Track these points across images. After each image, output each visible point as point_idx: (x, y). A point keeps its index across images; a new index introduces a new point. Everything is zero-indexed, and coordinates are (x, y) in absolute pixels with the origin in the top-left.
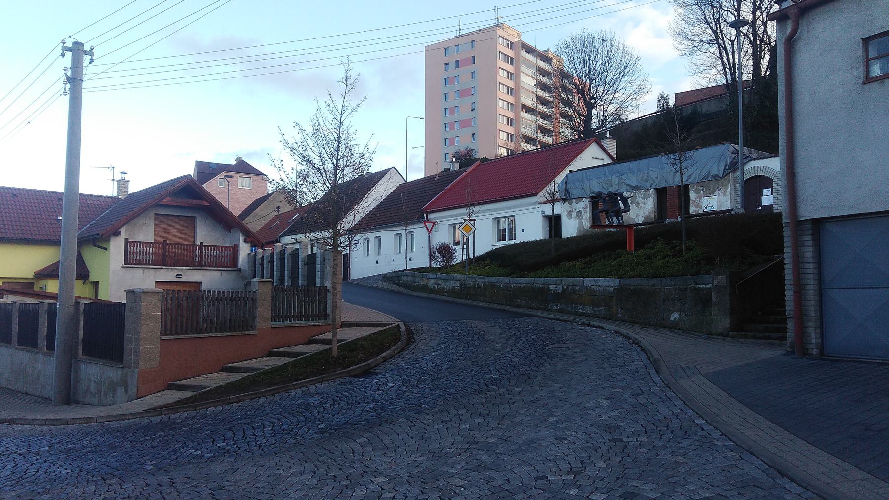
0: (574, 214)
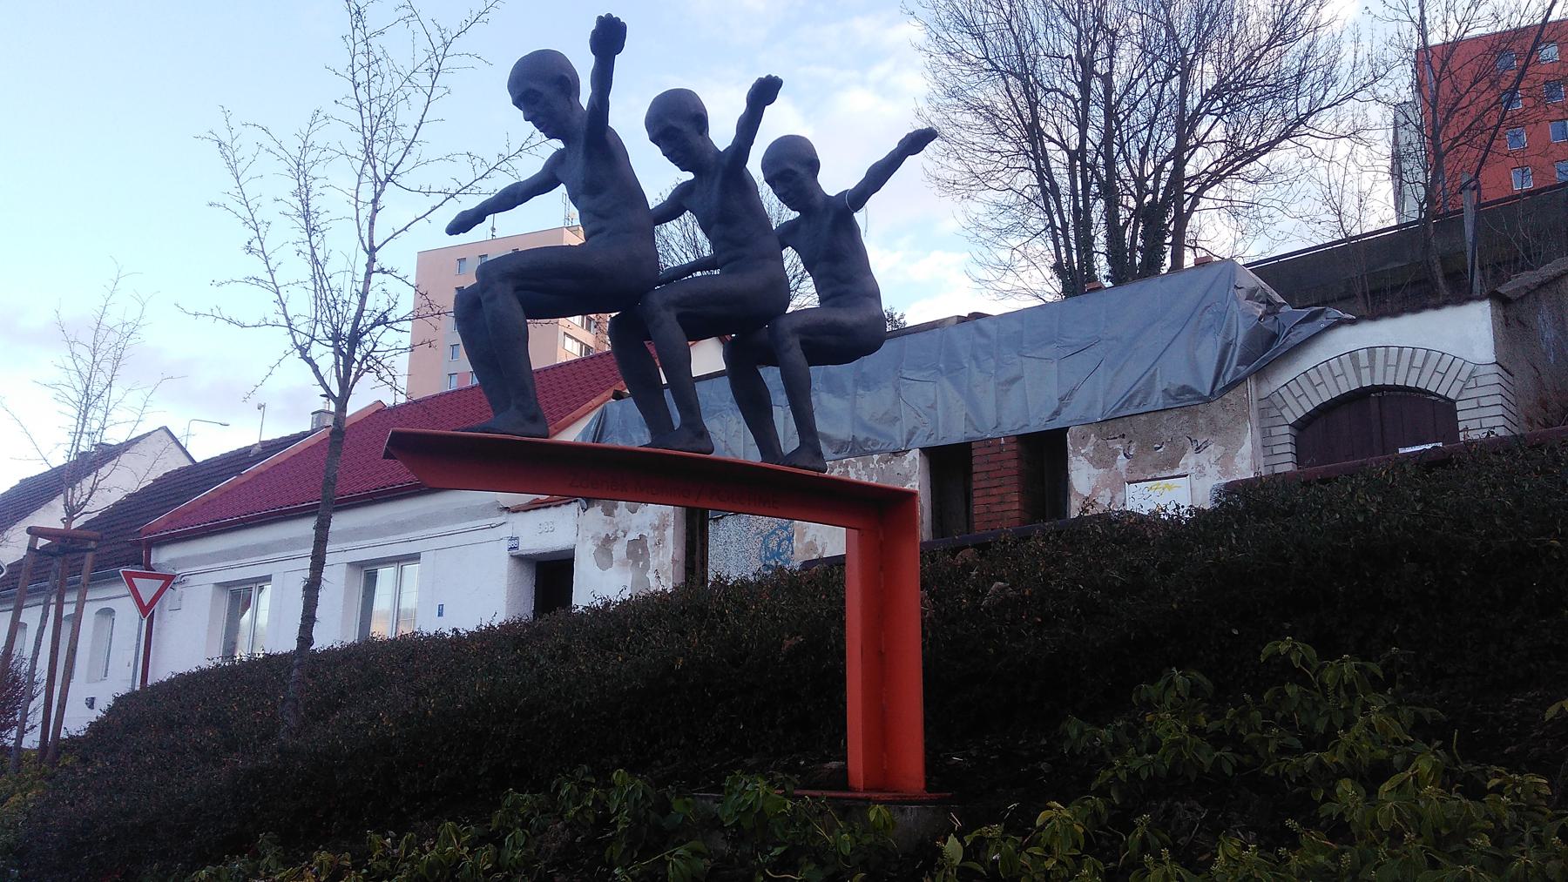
0: (619, 550)
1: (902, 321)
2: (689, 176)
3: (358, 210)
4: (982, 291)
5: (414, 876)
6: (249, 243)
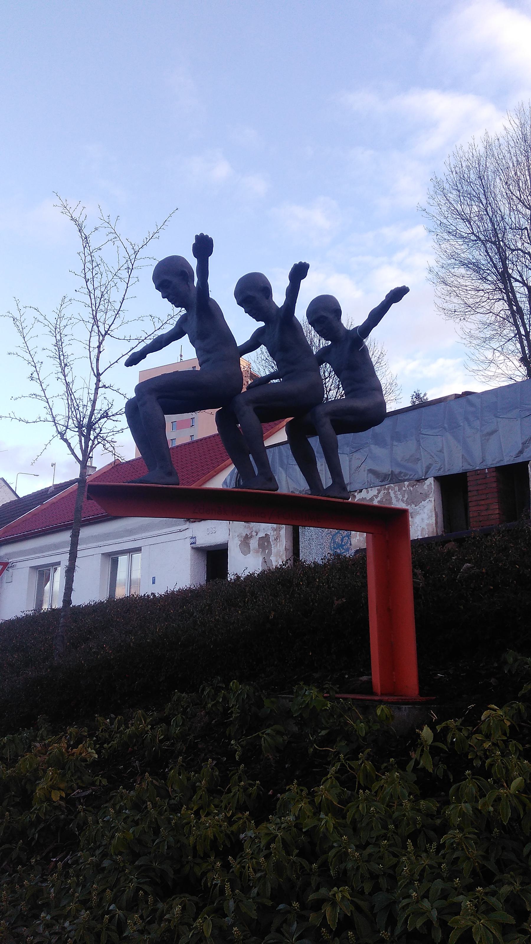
0: (254, 543)
1: (425, 398)
2: (262, 324)
3: (90, 352)
4: (475, 377)
5: (122, 742)
6: (32, 374)
